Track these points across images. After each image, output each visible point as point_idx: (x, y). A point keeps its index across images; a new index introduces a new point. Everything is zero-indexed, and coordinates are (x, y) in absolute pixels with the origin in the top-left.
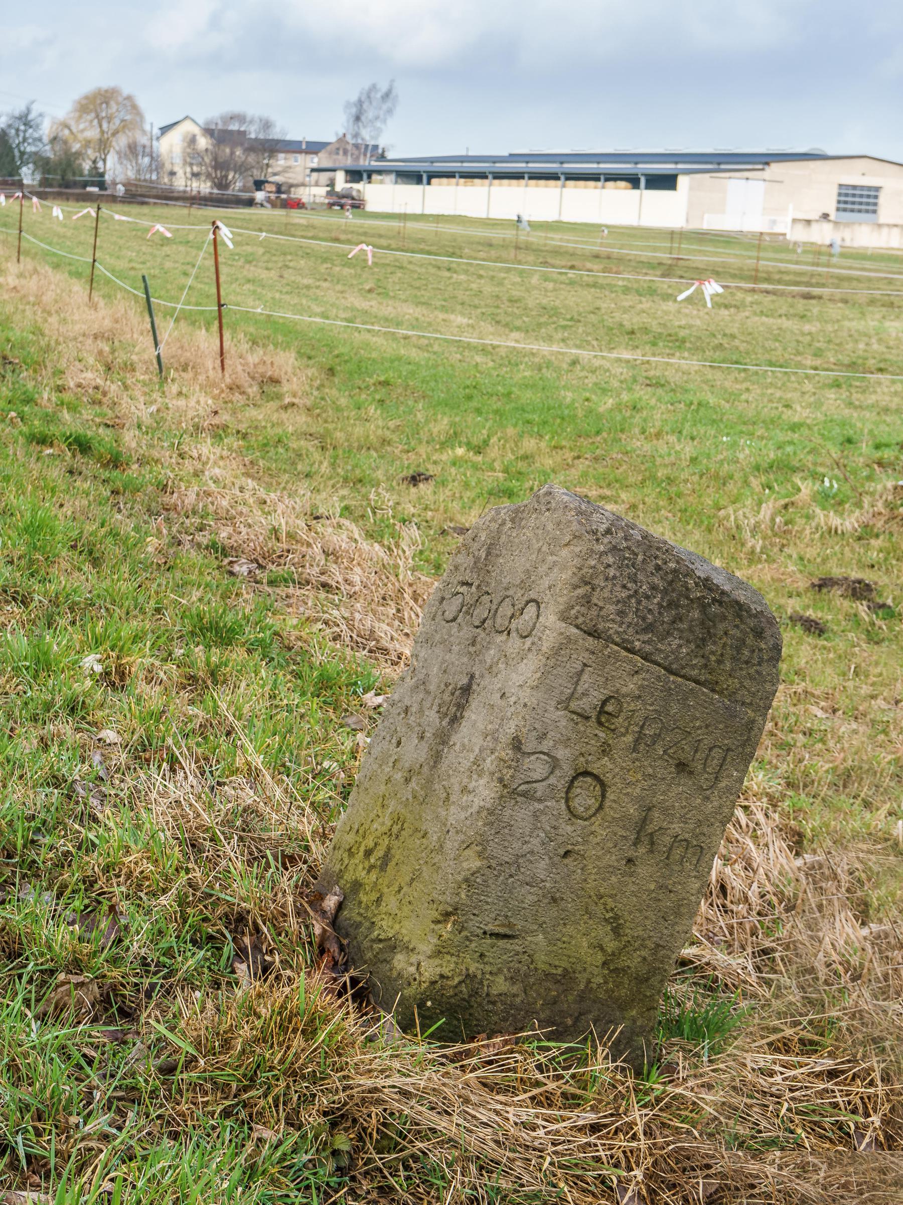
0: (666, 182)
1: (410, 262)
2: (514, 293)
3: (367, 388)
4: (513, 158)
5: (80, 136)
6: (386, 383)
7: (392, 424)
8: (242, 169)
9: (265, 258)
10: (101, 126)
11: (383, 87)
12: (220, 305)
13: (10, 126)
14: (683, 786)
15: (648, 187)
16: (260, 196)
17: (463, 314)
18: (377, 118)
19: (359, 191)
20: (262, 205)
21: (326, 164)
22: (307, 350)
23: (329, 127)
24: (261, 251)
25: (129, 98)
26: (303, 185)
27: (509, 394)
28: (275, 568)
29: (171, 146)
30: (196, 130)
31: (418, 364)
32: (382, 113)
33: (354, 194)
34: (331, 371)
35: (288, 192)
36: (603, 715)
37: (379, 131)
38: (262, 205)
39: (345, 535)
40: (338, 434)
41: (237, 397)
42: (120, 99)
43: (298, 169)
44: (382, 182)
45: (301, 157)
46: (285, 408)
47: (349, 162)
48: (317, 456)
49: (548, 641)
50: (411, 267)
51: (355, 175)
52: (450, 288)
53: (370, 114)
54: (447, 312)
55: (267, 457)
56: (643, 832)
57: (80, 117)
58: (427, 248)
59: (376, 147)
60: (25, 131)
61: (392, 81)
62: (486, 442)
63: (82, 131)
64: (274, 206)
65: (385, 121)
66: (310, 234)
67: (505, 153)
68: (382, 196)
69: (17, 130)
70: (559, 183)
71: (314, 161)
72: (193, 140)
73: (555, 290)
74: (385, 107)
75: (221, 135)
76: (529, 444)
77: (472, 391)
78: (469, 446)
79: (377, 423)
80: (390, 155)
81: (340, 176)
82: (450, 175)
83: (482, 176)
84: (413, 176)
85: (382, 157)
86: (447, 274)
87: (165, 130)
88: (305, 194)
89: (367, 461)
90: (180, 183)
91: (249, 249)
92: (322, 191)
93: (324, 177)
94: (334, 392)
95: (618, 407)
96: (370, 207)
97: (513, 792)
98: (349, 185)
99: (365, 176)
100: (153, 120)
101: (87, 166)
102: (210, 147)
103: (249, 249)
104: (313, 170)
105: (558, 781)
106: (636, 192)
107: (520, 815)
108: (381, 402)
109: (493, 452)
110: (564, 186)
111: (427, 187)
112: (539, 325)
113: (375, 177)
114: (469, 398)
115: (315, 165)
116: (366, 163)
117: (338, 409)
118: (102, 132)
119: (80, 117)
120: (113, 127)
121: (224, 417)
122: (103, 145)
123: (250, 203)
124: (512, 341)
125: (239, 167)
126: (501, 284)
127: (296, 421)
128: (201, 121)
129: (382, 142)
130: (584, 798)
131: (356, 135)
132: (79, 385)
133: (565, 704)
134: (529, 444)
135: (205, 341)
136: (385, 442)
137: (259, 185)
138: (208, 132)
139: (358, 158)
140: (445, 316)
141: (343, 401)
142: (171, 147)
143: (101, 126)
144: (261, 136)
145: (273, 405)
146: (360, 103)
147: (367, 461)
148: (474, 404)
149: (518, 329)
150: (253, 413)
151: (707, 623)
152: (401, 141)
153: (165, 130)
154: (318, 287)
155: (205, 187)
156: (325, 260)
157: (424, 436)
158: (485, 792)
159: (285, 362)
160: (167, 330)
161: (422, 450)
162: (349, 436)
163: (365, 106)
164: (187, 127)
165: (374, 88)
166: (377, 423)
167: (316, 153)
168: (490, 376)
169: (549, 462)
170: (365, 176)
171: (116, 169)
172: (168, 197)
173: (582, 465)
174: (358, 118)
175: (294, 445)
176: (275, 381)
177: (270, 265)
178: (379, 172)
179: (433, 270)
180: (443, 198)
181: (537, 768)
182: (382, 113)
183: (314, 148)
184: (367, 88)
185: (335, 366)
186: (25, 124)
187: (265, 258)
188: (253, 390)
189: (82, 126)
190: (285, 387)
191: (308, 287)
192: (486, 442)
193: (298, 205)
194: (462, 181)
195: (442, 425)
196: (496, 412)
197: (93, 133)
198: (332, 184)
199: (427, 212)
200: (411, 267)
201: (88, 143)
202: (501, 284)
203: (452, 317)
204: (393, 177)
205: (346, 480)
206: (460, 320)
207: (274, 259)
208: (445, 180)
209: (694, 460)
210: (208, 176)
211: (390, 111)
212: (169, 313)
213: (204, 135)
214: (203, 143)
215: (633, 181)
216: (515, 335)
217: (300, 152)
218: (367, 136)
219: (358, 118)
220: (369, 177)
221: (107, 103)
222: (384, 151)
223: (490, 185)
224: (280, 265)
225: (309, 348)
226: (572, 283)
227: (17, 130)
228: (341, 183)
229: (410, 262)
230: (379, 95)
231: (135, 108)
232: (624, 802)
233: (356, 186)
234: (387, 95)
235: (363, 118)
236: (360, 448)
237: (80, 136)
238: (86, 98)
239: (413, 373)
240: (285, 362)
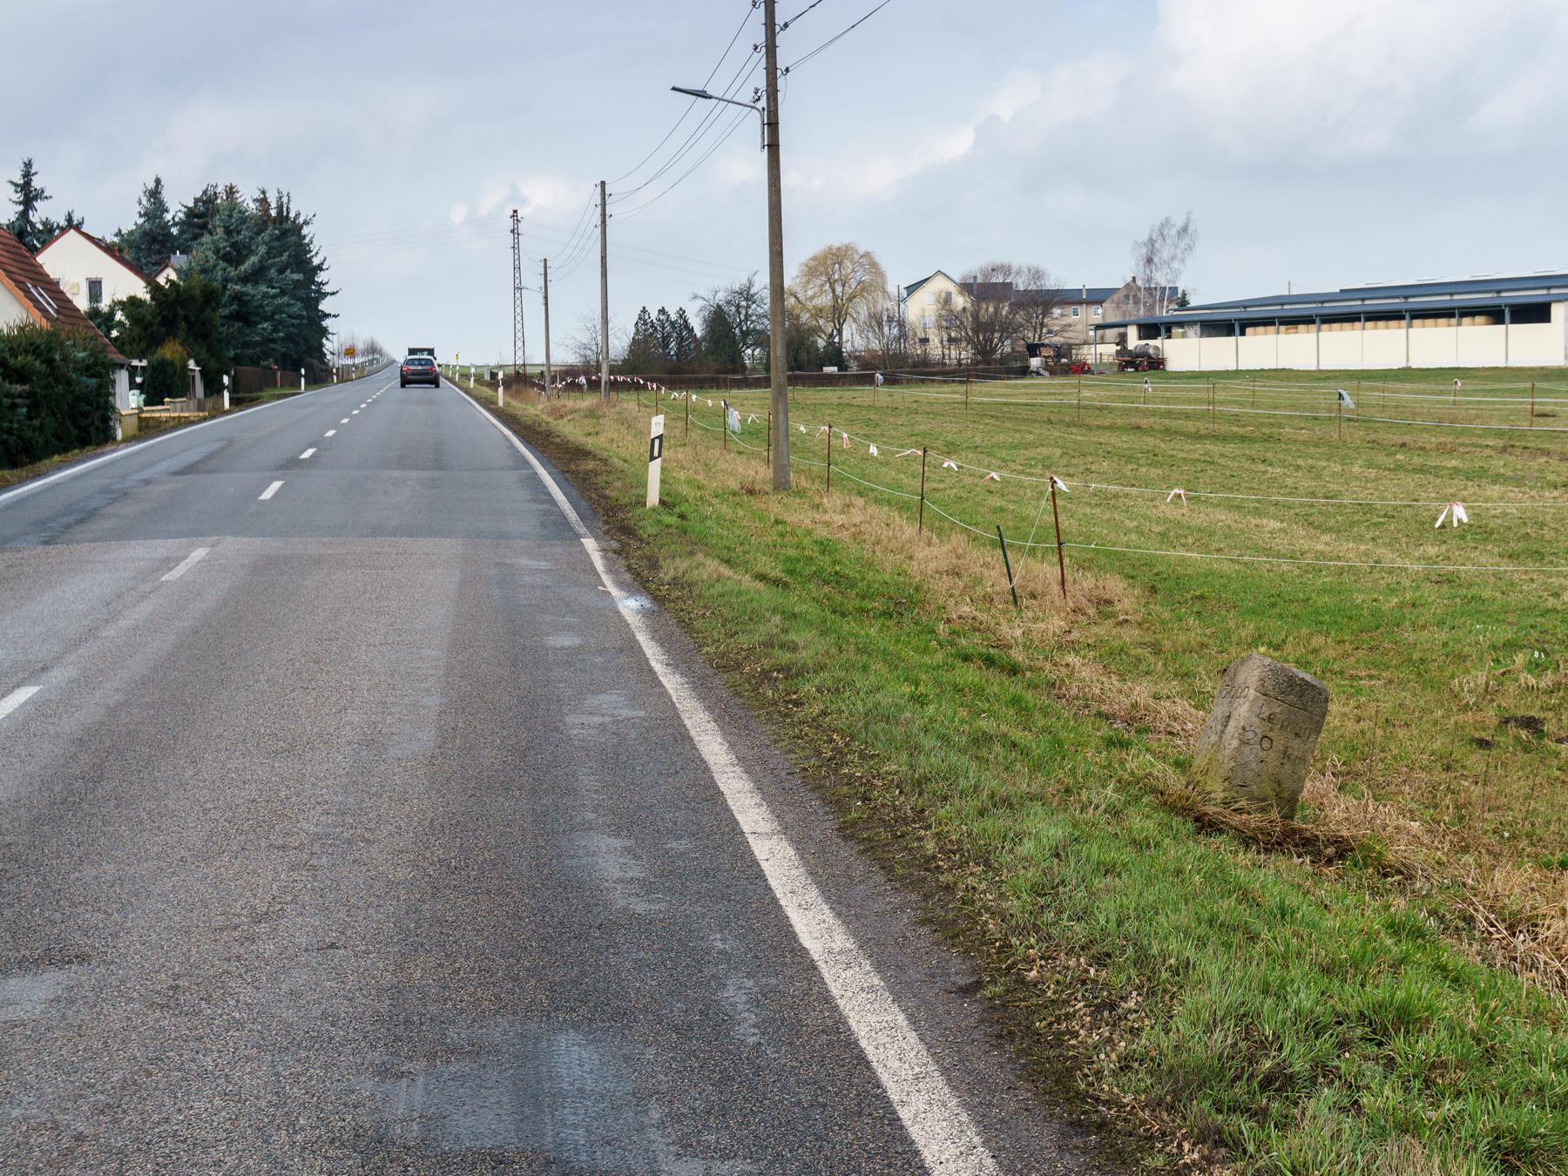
0: (1537, 313)
1: (1222, 455)
2: (1331, 486)
3: (1186, 602)
4: (1346, 294)
5: (810, 305)
6: (1201, 597)
7: (1208, 632)
8: (1008, 329)
9: (1064, 461)
10: (834, 291)
11: (1179, 224)
12: (1060, 544)
13: (729, 303)
14: (1298, 740)
15: (1514, 321)
16: (1035, 362)
17: (1275, 517)
18: (1173, 258)
19: (1157, 348)
20: (1038, 373)
21: (1111, 319)
22: (1128, 570)
23: (1114, 271)
24: (1059, 452)
25: (867, 255)
26: (1086, 343)
27: (1308, 600)
28: (1137, 720)
29: (923, 310)
30: (952, 288)
31: (1229, 577)
32: (1179, 252)
33: (1151, 351)
34: (1154, 590)
35: (1068, 354)
36: (1270, 719)
37: (1177, 273)
38: (1038, 373)
39: (1182, 707)
40: (57, 788)
41: (1081, 618)
42: (856, 257)
43: (1079, 327)
44: (1184, 336)
45: (1082, 309)
46: (1120, 624)
47: (1142, 314)
48: (1152, 659)
49: (1251, 697)
50: (1222, 461)
51: (1150, 330)
52: (1264, 487)
53: (1165, 254)
54: (1260, 516)
55: (1112, 658)
56: (1285, 754)
57: (808, 282)
58: (1241, 431)
59: (1174, 290)
60: (748, 307)
61: (1189, 213)
62: (1284, 641)
63: (812, 298)
64: (1053, 372)
65: (1183, 260)
66: (1106, 422)
67: (1335, 288)
68: (1186, 352)
69: (738, 307)
70: (1404, 323)
71: (1096, 315)
72: (948, 299)
73: (1376, 479)
74: (1182, 245)
75: (980, 290)
76: (1317, 641)
77: (1276, 600)
78: (1270, 645)
79: (1195, 631)
80: (1194, 301)
81: (1132, 332)
82: (1267, 322)
83: (1308, 320)
84: (1225, 324)
85: (1183, 303)
86: (1261, 467)
87: (912, 289)
88: (1089, 354)
89: (1190, 661)
90: (935, 349)
91: (1045, 451)
92: (1111, 349)
93: (1111, 334)
94: (1158, 607)
95: (1401, 606)
96: (1172, 366)
97: (1244, 743)
98: (1143, 342)
99: (1163, 331)
100: (896, 281)
101: (821, 343)
102: (968, 305)
103: (1045, 451)
104: (1098, 327)
105: (1257, 739)
106: (1501, 327)
107: (1247, 749)
108: (1199, 613)
109: (1289, 647)
110: (1410, 326)
111: (1241, 338)
112: (1353, 524)
113: (1176, 331)
114: (1273, 605)
115: (1098, 319)
116: (1165, 312)
117: (1163, 622)
118: (835, 297)
119: (808, 282)
120: (848, 290)
121: (1075, 635)
122: (838, 314)
123: (1025, 372)
124: (1323, 543)
125: (1005, 330)
126: (1319, 477)
127: (1130, 635)
128: (957, 278)
129: (1181, 286)
130: (1266, 744)
131: (1149, 280)
132: (960, 617)
133: (1258, 716)
134: (1317, 641)
135: (1048, 571)
136: (1203, 646)
137: (1033, 350)
138: (966, 287)
139: (1152, 307)
140: (1257, 521)
141: (1166, 615)
142: (921, 310)
143: (834, 291)
144: (1033, 287)
145: (1111, 621)
146: (1152, 241)
147: (1190, 661)
148: (1277, 610)
149: (1330, 530)
150: (1096, 629)
151: (1302, 692)
152: (1208, 285)
153: (912, 289)
154: (1126, 495)
155: (966, 354)
156: (1130, 459)
157: (1234, 638)
158: (1235, 743)
159: (1115, 585)
160: (1019, 565)
161: (1232, 650)
162: (1174, 642)
163: (1157, 245)
164: (940, 285)
165: (1167, 222)
166: (1195, 631)
167: (1100, 303)
168: (1293, 583)
169: (1332, 653)
170: (1163, 331)
171: (853, 339)
172: (924, 371)
173: (1360, 654)
174: (1149, 261)
175: (1133, 652)
176: (1109, 602)
177: (1071, 470)
178: (1180, 324)
179: (1246, 464)
180: (1261, 350)
181: (1251, 735)
182: (1179, 252)
183: (1096, 298)
184: (1158, 223)
185: (1158, 584)
186: (746, 299)
187: (1064, 461)
188: (1092, 611)
189: (810, 293)
190: (1119, 607)
191: (1116, 496)
192: (1284, 641)
193: (1081, 369)
194: (1283, 328)
195: (1250, 629)
196: (1295, 616)
197: (825, 300)
198: (1122, 340)
199: (1242, 367)
200: (1222, 461)
201: (819, 312)
202: (1319, 477)
203: (1265, 521)
204: (1198, 328)
205: (1176, 675)
206: (1274, 524)
207: (1074, 461)
208: (1261, 329)
209: (1445, 644)
210: (969, 340)
211: (1189, 248)
212: (1011, 545)
213: (961, 293)
214: (960, 302)
215: (1495, 315)
216: (1327, 538)
217: (1080, 303)
218: (1162, 279)
219: (1149, 261)
220: (1169, 331)
221: (840, 263)
222: (1184, 295)
223: (1319, 330)
224: (1082, 468)
225: (1131, 569)
226: (1398, 468)
227: (738, 307)
228: (1133, 341)
229: (1222, 455)
230: (1174, 232)
231: (874, 265)
232: (1279, 745)
233: (1152, 342)
234: (1185, 229)
235: (1156, 260)
236: (1184, 652)
237: (810, 305)
238: (815, 259)
239: (1225, 586)
240: (1115, 585)
